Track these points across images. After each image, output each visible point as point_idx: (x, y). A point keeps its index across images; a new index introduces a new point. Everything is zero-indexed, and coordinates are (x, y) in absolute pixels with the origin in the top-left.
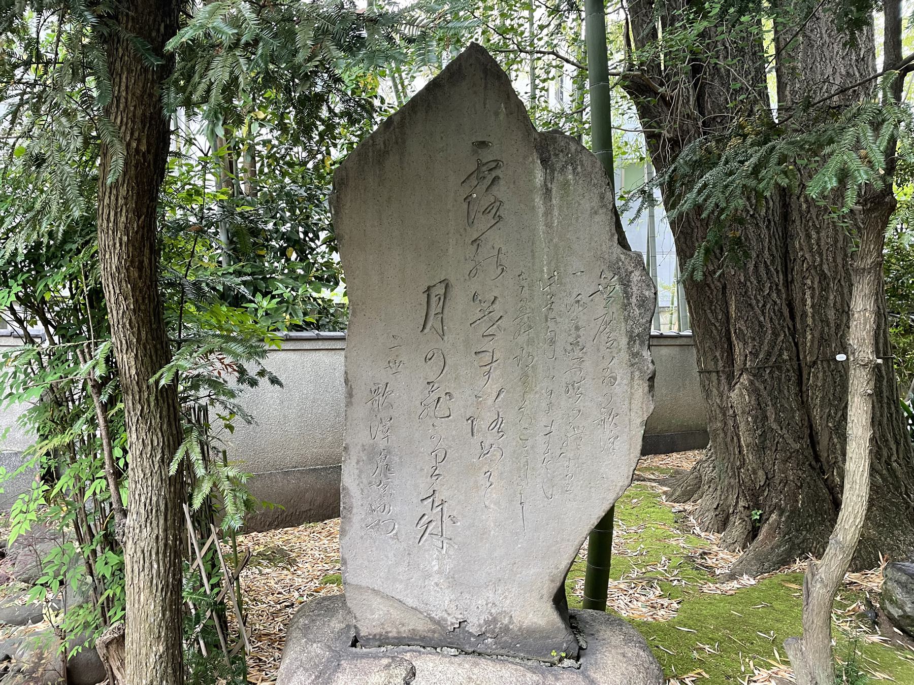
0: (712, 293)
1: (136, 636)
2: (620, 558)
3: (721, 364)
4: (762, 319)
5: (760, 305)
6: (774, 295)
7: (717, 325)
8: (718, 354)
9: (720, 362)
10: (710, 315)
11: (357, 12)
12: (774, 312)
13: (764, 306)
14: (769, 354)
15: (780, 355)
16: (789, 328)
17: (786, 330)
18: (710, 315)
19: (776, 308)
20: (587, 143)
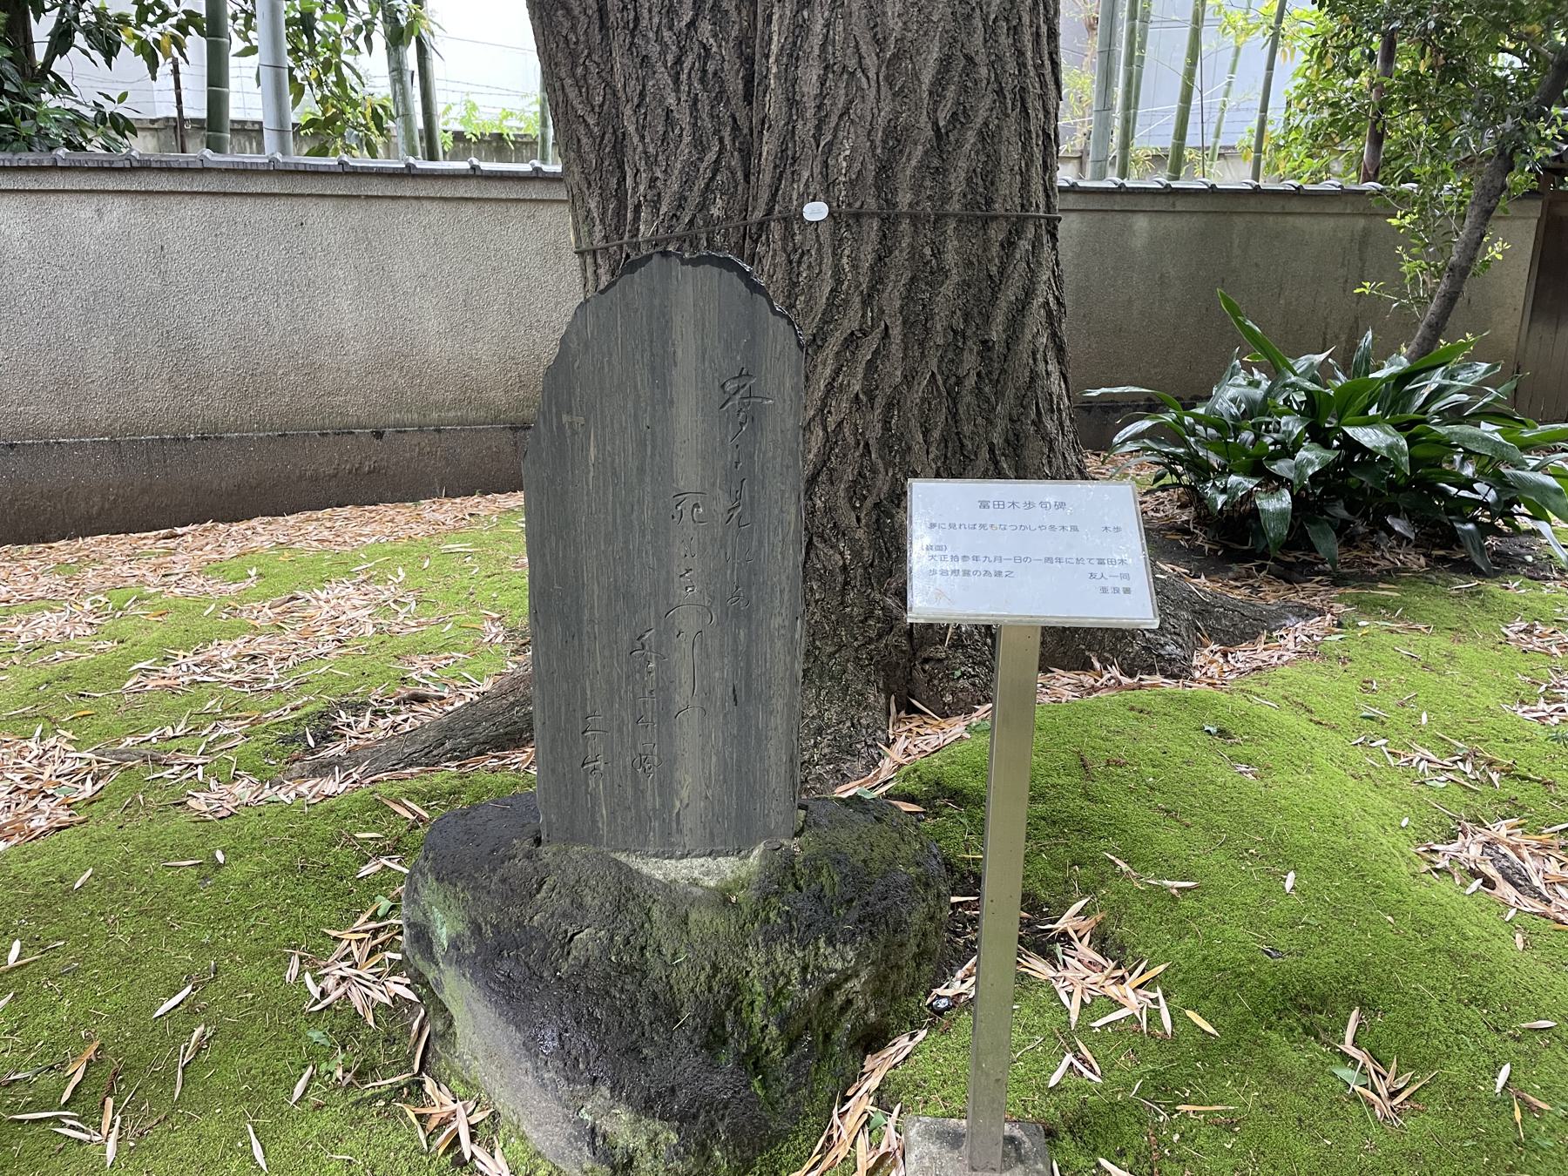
0: (573, 28)
1: (340, 602)
2: (503, 550)
3: (598, 233)
4: (671, 100)
5: (670, 59)
6: (705, 27)
7: (591, 122)
8: (593, 205)
9: (598, 227)
10: (572, 94)
11: (911, 618)
12: (702, 81)
13: (678, 61)
14: (681, 202)
15: (703, 206)
16: (736, 128)
17: (726, 133)
18: (572, 94)
19: (711, 68)
20: (1255, 384)
